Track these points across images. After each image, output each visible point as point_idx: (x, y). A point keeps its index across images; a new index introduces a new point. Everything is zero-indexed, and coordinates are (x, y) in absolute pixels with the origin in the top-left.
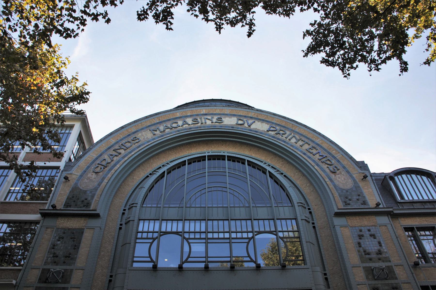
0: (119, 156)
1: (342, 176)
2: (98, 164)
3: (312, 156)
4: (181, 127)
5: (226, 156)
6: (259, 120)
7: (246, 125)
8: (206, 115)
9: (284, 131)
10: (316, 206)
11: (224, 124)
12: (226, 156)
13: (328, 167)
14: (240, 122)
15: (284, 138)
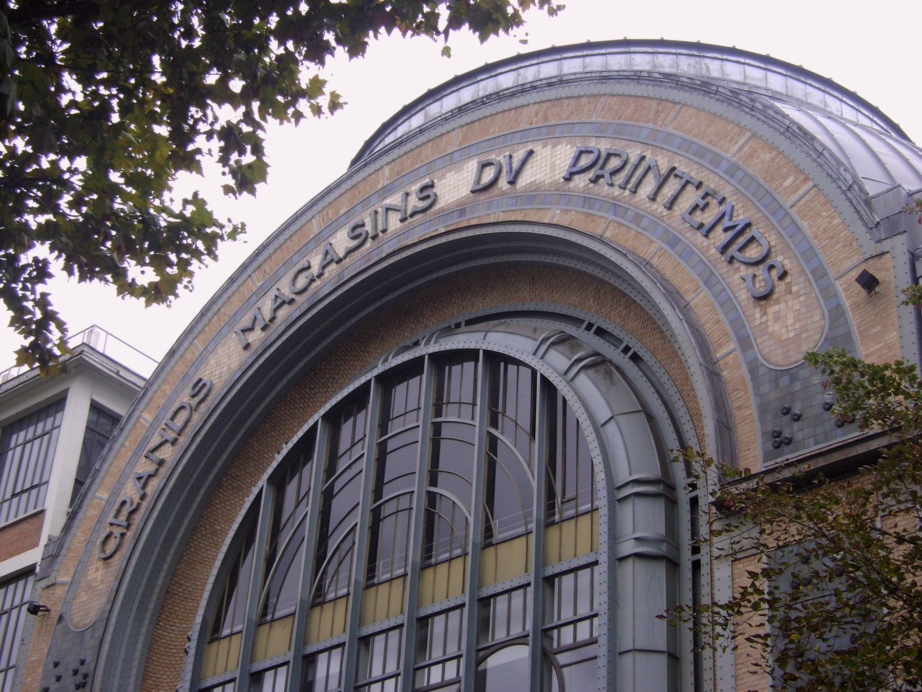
2: (111, 524)
5: (481, 353)
12: (481, 353)
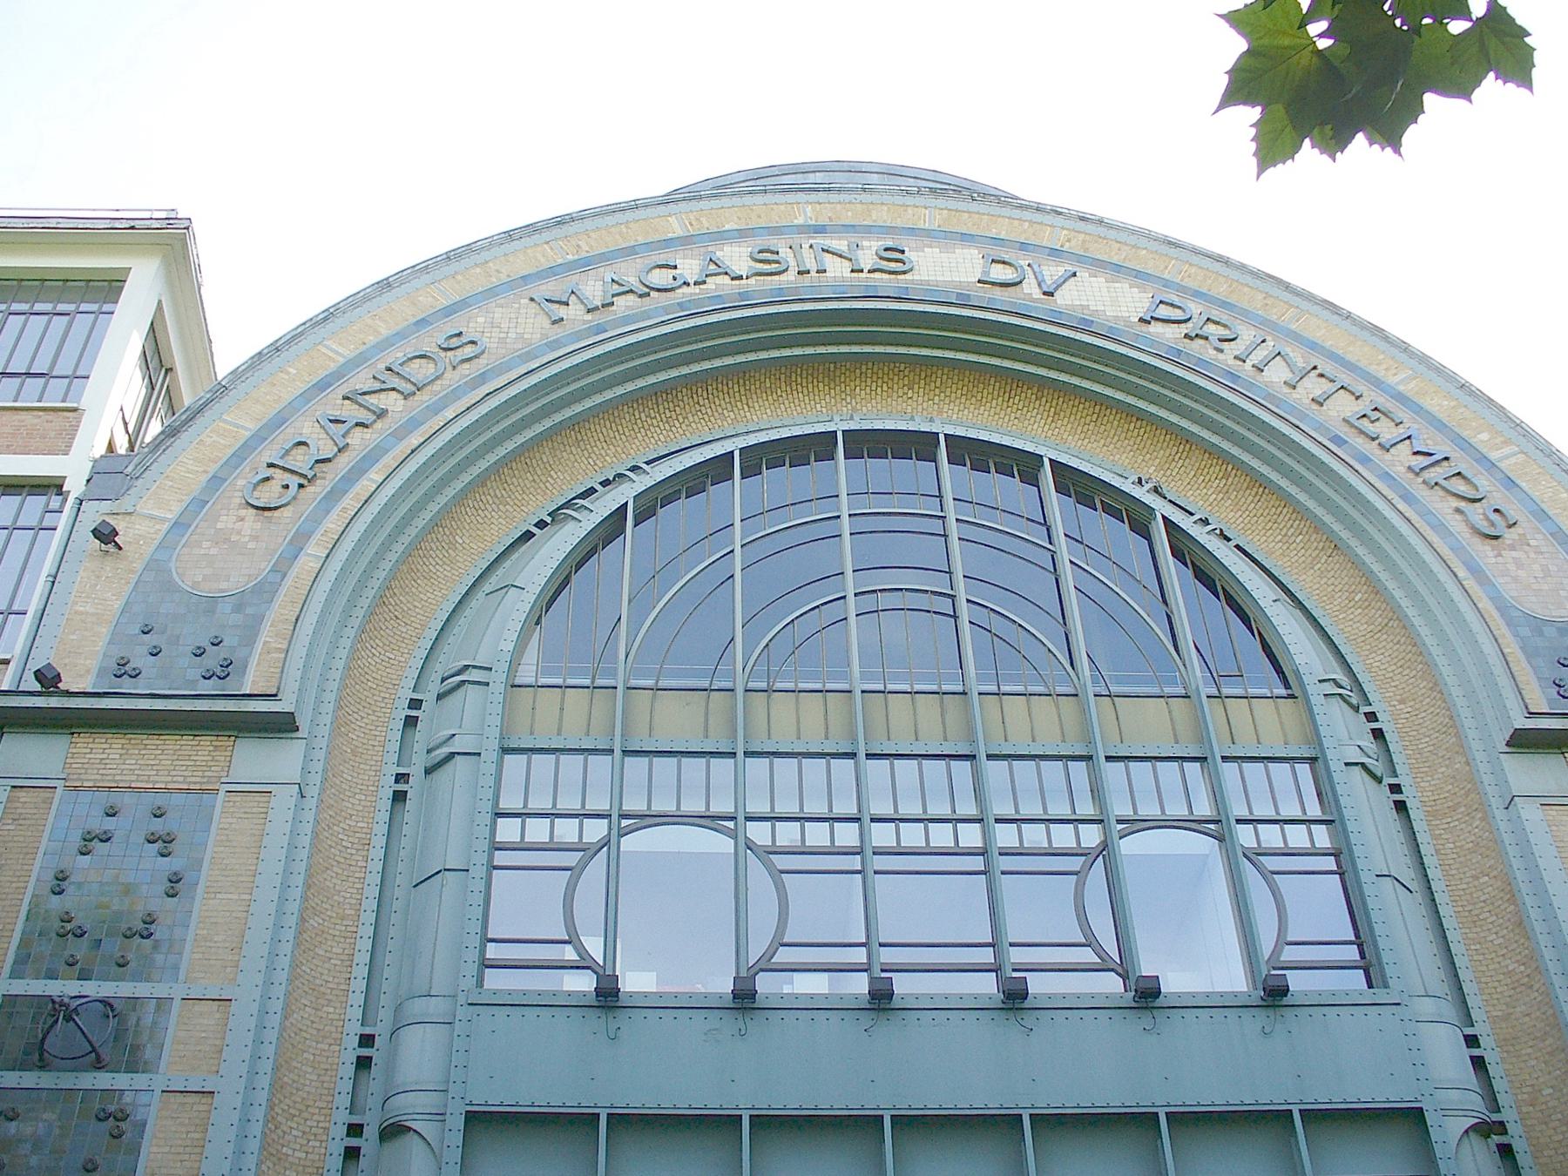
0: (379, 425)
1: (1532, 555)
2: (271, 465)
3: (1378, 452)
4: (697, 289)
6: (1099, 265)
7: (1030, 288)
8: (820, 230)
9: (1225, 326)
10: (1402, 702)
11: (915, 278)
13: (1458, 510)
14: (1000, 273)
15: (1227, 358)
